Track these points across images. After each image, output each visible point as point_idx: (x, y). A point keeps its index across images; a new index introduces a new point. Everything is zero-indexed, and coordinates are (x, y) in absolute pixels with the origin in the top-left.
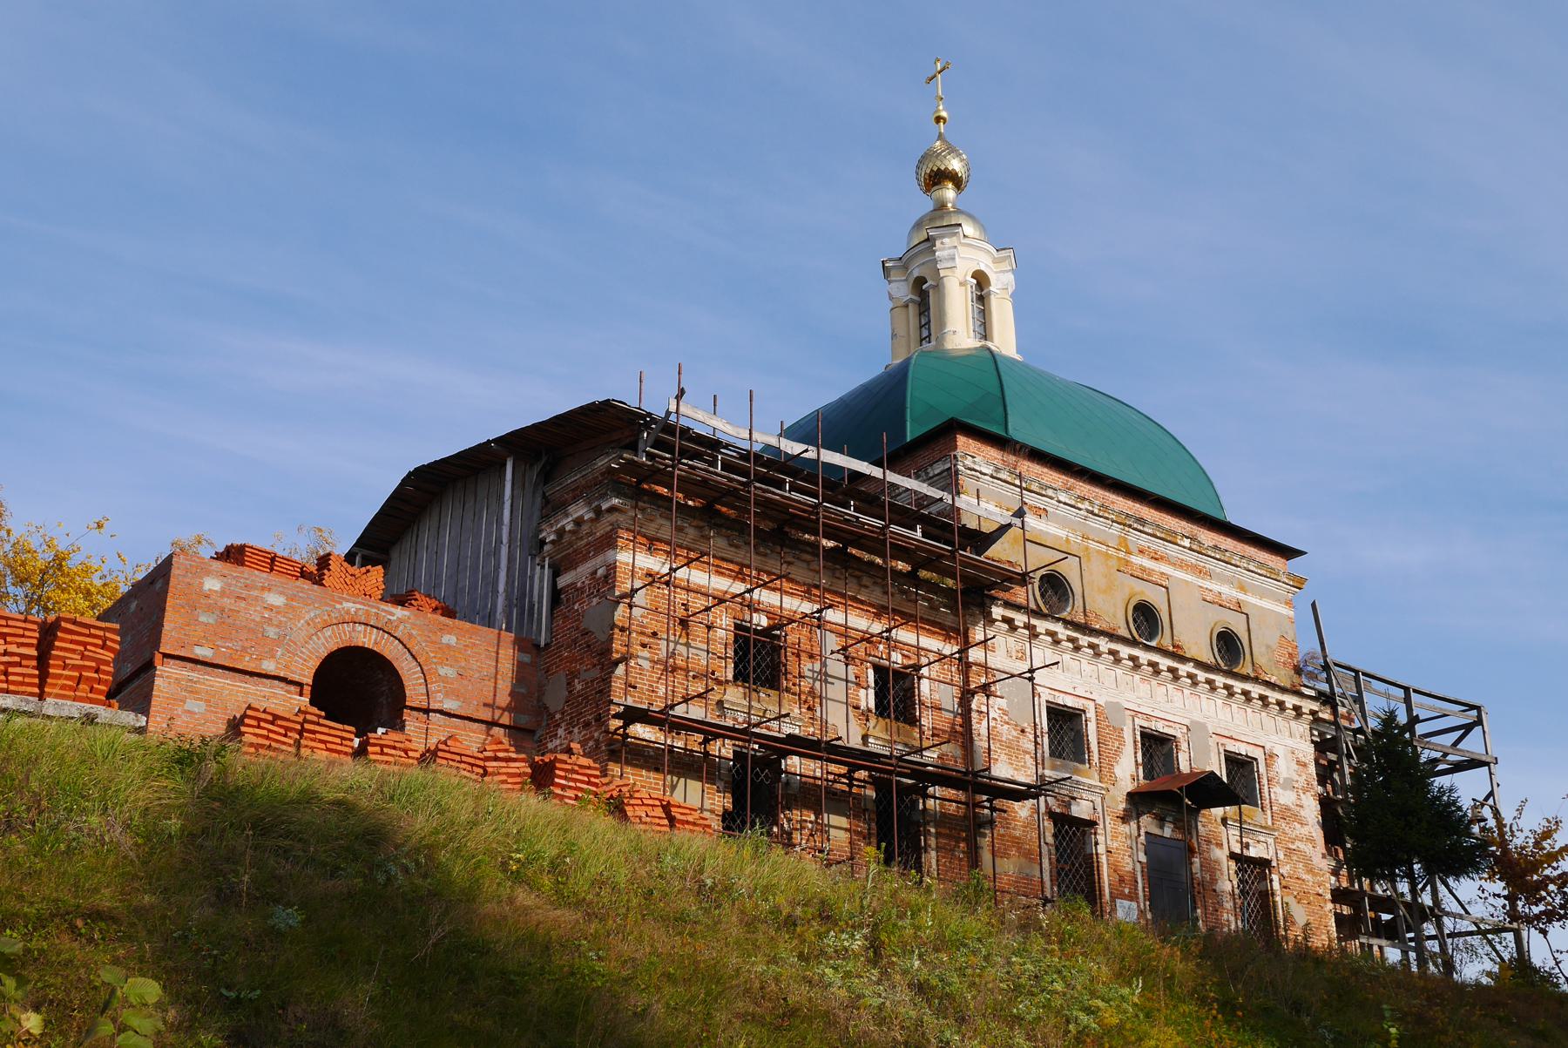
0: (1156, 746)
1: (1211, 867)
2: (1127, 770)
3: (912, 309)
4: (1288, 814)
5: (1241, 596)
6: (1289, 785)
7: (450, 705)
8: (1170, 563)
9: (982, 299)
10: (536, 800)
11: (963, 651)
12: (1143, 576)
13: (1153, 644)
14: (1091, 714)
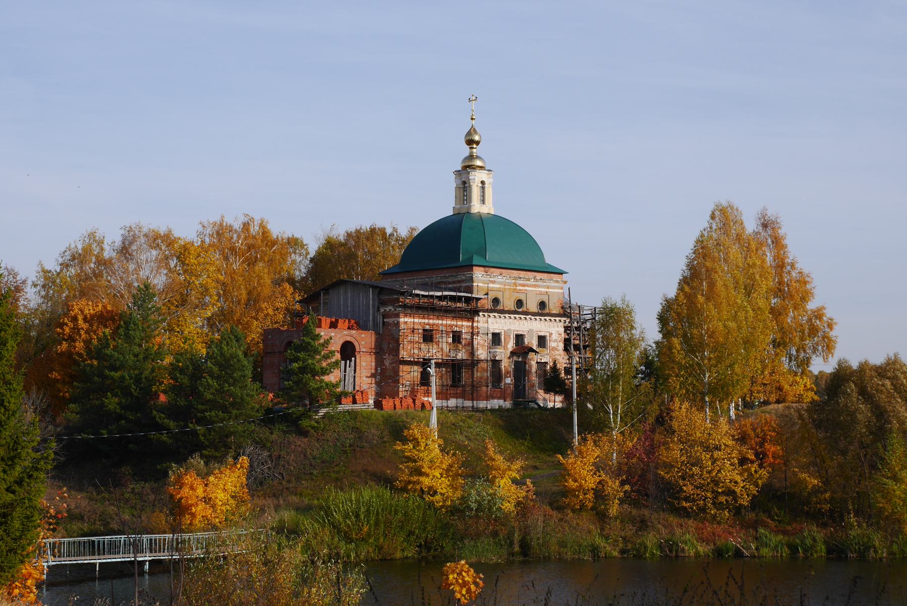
0: (519, 338)
1: (530, 366)
2: (511, 345)
3: (462, 190)
4: (554, 349)
5: (548, 290)
6: (555, 341)
7: (364, 350)
8: (528, 286)
9: (483, 188)
10: (282, 274)
11: (473, 324)
12: (520, 291)
13: (520, 310)
14: (503, 333)
